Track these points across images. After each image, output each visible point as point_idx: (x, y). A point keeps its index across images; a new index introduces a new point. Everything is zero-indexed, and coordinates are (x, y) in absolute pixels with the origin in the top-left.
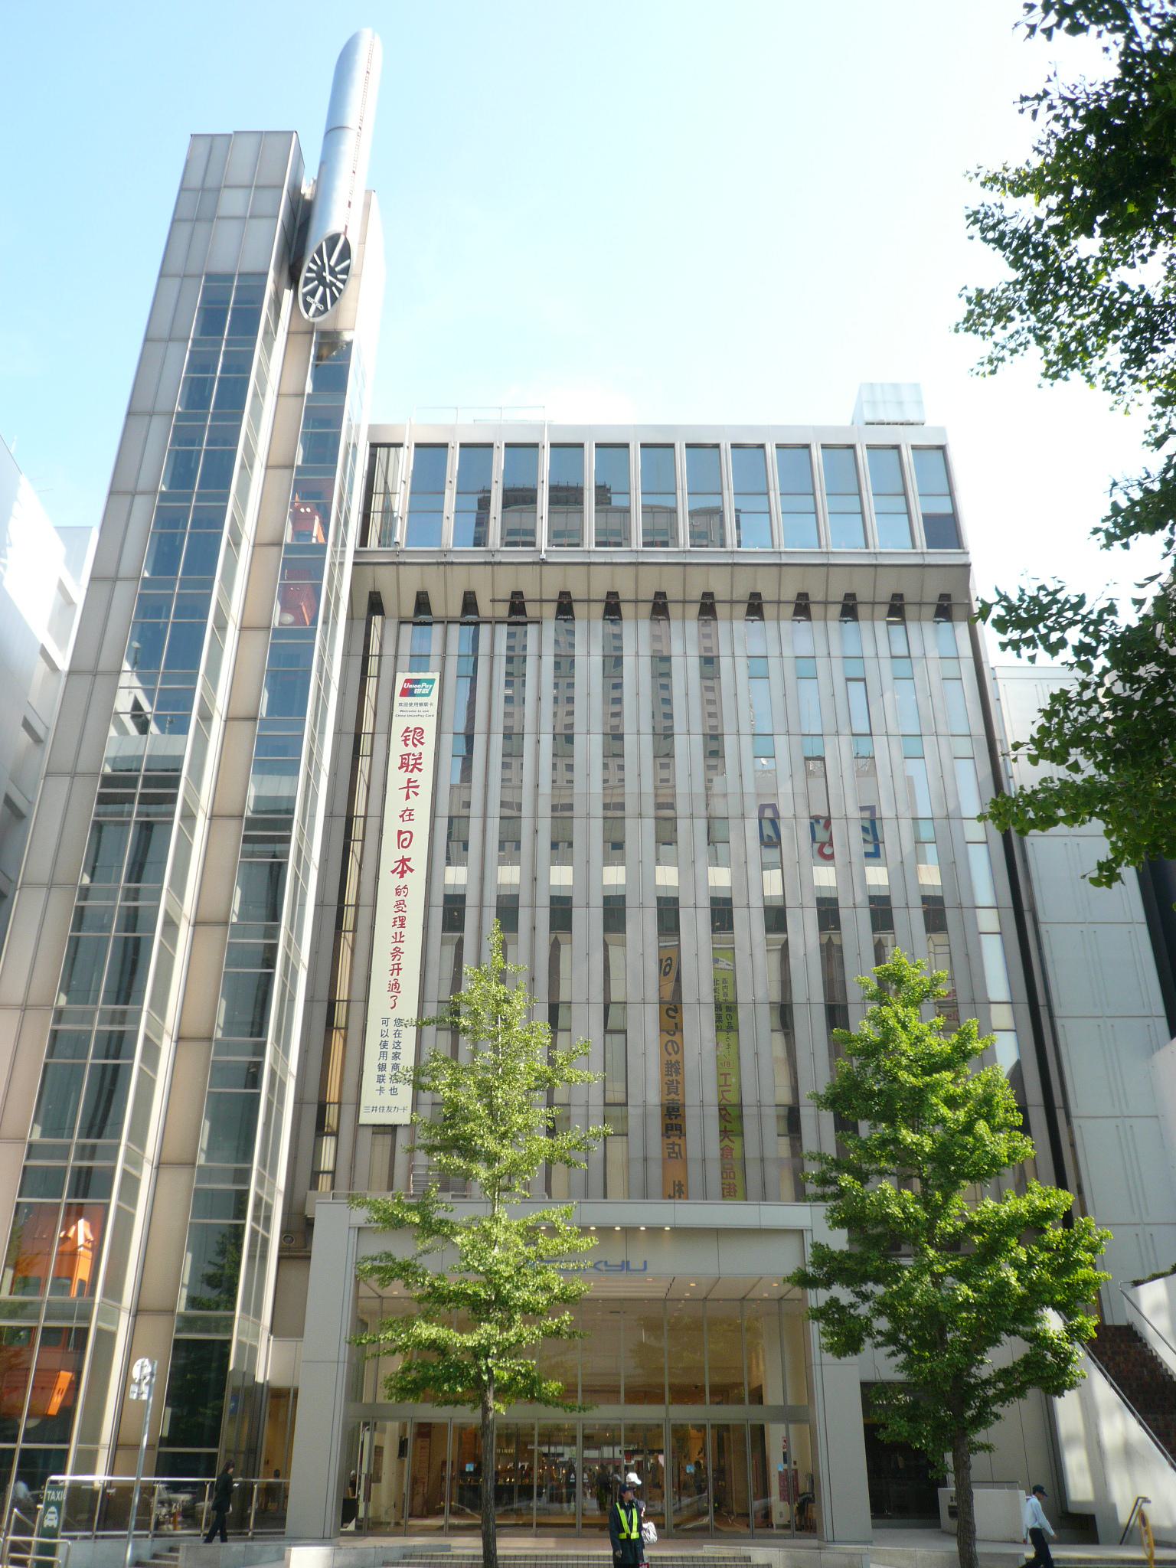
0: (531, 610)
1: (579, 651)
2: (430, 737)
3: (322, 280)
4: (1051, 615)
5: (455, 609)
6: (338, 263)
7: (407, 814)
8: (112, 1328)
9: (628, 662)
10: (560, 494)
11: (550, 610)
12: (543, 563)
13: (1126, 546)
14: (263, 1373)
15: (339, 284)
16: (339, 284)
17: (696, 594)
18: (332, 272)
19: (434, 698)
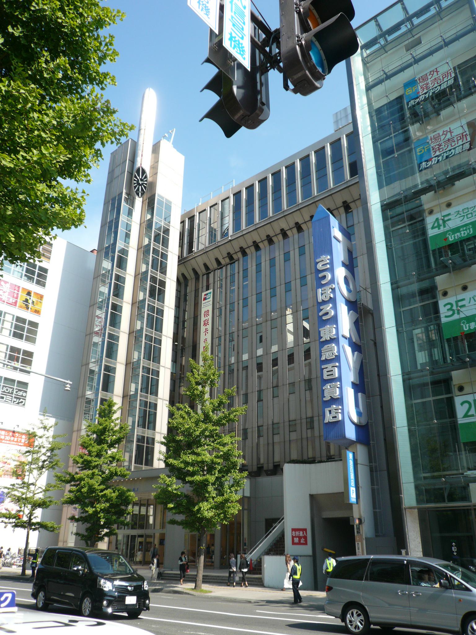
0: (235, 257)
1: (249, 266)
2: (210, 313)
3: (139, 184)
4: (68, 157)
5: (215, 265)
6: (142, 177)
7: (206, 340)
8: (445, 400)
9: (263, 264)
10: (399, 210)
11: (240, 255)
12: (230, 241)
13: (104, 63)
14: (146, 589)
15: (145, 182)
16: (145, 182)
17: (278, 231)
18: (142, 180)
19: (211, 299)
